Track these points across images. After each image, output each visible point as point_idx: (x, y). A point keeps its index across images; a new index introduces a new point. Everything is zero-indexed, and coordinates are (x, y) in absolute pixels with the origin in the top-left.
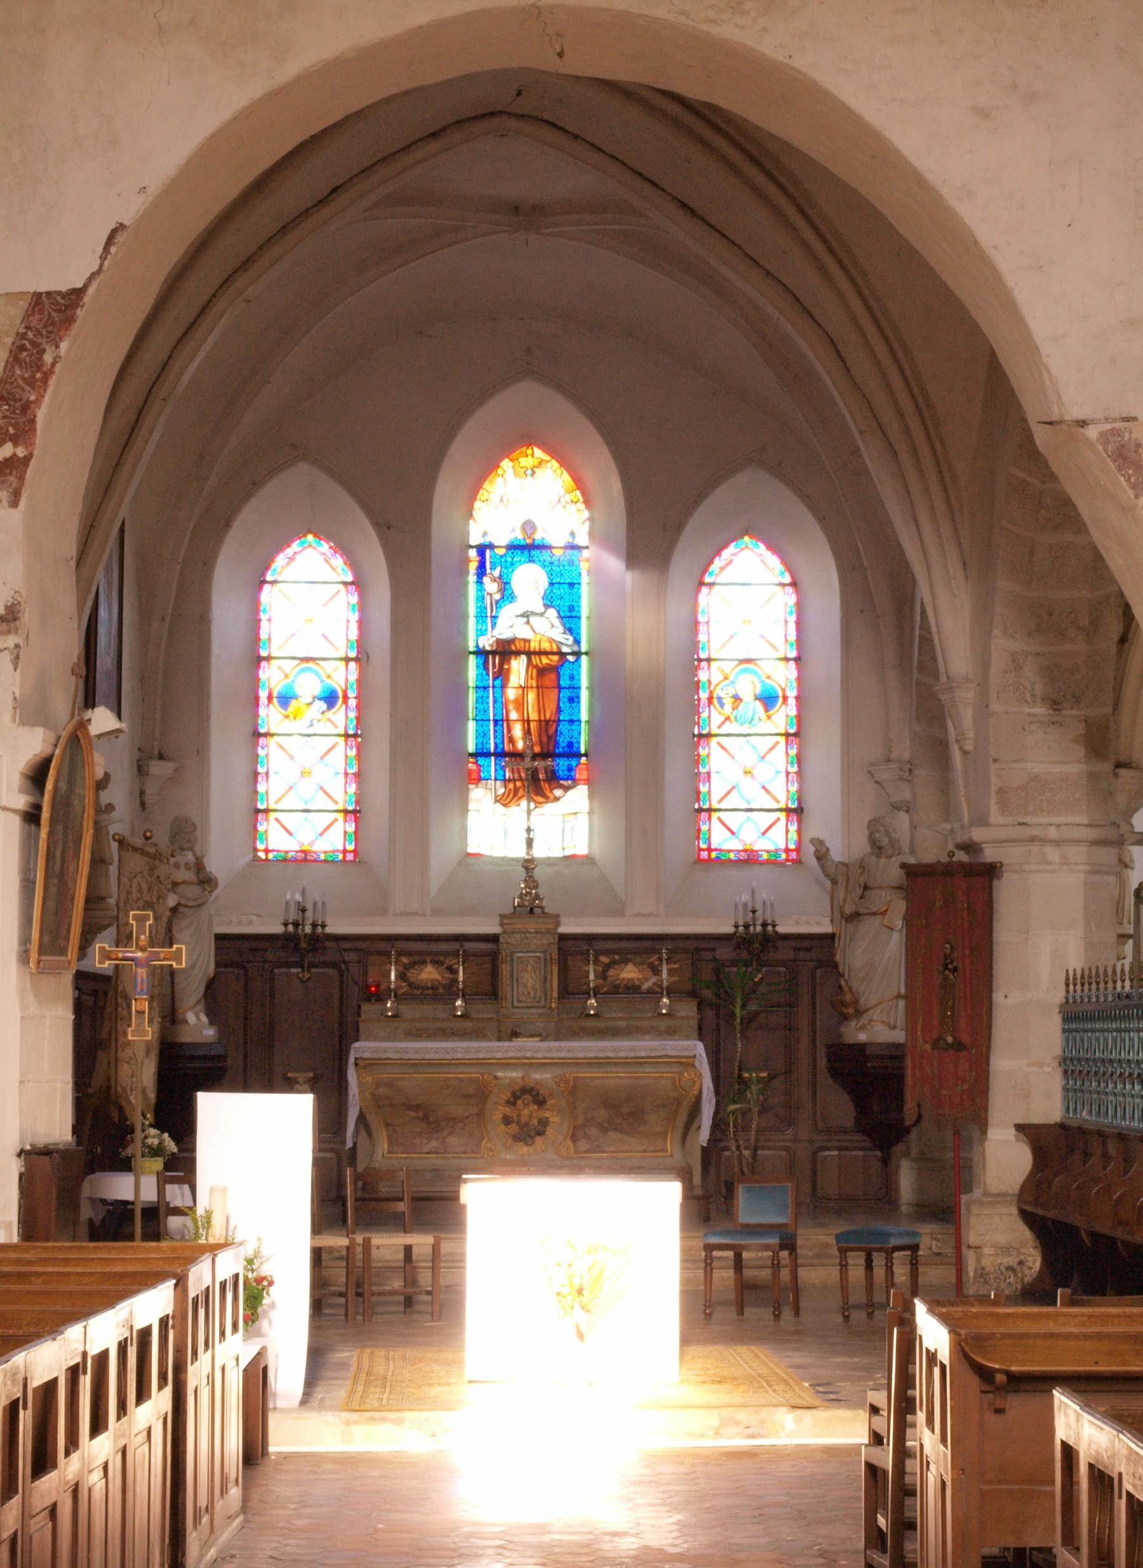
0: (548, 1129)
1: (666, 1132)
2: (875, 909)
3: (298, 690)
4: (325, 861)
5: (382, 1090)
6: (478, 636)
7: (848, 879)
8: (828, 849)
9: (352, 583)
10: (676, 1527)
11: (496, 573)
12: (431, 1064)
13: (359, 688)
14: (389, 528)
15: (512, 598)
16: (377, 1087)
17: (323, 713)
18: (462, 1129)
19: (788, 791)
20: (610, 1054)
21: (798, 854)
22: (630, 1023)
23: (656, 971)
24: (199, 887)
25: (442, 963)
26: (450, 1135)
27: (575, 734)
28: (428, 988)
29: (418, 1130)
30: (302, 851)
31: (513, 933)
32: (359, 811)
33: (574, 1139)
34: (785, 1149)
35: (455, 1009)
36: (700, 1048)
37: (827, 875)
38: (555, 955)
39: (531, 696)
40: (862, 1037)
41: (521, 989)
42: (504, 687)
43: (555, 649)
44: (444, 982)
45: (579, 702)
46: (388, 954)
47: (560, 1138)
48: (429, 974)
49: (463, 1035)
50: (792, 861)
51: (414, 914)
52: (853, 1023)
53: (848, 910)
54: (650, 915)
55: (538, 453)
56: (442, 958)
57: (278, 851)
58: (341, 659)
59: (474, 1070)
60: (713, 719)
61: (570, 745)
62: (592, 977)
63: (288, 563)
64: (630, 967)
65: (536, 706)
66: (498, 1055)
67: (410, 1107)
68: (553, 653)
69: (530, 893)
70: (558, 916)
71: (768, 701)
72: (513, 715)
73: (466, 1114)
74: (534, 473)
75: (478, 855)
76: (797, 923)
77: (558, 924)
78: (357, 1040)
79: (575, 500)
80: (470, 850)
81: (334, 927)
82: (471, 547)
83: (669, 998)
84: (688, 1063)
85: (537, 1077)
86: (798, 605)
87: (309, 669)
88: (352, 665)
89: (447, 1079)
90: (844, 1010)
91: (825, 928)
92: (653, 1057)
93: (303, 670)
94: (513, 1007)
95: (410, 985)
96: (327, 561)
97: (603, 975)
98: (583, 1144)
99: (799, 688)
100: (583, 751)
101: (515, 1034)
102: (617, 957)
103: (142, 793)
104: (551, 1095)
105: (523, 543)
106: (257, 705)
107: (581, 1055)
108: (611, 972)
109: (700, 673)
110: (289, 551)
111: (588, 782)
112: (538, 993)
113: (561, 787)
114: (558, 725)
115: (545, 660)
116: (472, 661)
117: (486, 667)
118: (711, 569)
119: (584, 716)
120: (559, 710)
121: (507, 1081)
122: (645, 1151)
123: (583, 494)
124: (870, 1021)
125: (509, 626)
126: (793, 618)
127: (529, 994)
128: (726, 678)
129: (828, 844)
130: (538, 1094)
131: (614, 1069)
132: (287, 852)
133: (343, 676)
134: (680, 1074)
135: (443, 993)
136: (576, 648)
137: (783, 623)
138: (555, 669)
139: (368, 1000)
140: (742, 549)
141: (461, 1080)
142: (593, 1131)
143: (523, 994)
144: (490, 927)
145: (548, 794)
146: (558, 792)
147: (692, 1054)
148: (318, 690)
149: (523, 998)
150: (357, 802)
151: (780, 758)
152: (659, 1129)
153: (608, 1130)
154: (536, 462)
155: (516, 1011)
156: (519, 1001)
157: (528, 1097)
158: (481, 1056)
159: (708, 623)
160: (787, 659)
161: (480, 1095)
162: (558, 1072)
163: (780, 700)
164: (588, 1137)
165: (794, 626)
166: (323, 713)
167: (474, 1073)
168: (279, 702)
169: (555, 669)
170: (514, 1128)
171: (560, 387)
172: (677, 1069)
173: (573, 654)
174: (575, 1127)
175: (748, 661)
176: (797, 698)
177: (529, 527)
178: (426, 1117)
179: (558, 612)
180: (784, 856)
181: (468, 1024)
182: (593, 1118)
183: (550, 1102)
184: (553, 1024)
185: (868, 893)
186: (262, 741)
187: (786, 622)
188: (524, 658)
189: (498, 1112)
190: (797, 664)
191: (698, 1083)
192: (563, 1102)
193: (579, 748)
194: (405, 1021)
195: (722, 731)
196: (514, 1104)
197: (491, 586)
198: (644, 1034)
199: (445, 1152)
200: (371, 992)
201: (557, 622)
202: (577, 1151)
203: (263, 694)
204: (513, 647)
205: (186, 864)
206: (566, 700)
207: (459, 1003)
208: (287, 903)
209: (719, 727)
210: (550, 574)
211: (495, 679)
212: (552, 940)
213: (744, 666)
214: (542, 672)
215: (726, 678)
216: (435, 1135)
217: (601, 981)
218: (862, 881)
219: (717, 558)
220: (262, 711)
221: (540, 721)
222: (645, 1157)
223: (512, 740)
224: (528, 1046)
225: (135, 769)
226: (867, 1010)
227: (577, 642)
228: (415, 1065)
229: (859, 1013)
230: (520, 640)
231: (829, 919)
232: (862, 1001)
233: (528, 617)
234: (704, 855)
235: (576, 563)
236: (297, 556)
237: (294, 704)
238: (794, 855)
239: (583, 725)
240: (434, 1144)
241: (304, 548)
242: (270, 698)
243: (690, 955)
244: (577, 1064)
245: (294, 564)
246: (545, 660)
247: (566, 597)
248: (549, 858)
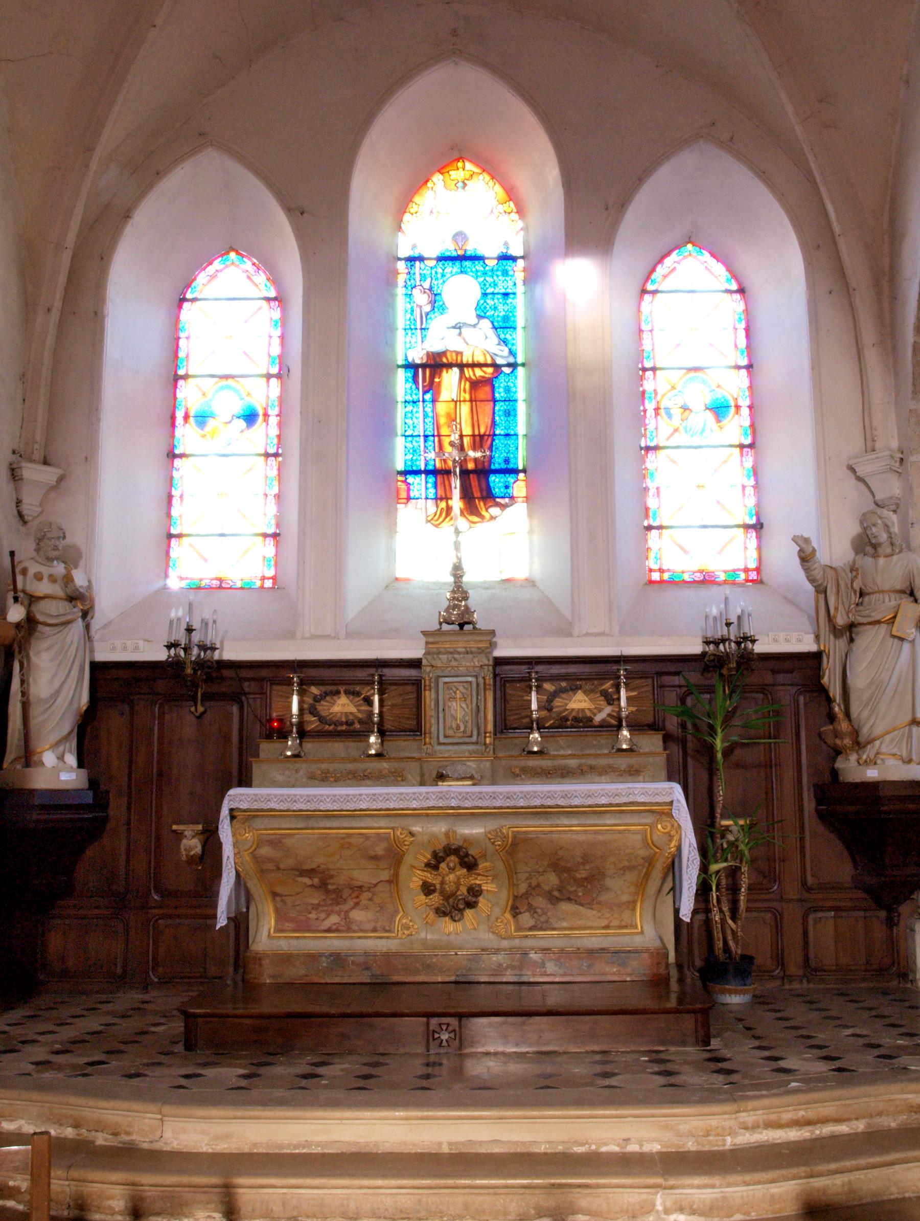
0: (481, 899)
1: (635, 902)
2: (877, 617)
3: (216, 408)
4: (242, 588)
5: (265, 851)
7: (838, 586)
8: (814, 550)
9: (275, 299)
12: (328, 815)
13: (281, 405)
14: (302, 214)
15: (443, 308)
16: (258, 846)
17: (242, 431)
18: (370, 900)
19: (683, 572)
20: (561, 802)
21: (758, 573)
22: (583, 761)
23: (612, 699)
24: (66, 603)
25: (358, 694)
26: (353, 908)
27: (512, 448)
28: (342, 724)
29: (315, 901)
30: (216, 579)
31: (439, 653)
32: (279, 535)
33: (515, 912)
34: (768, 910)
35: (369, 746)
36: (676, 792)
37: (812, 580)
38: (490, 681)
39: (465, 409)
40: (872, 774)
41: (449, 721)
42: (434, 401)
43: (489, 361)
44: (360, 715)
45: (515, 416)
46: (289, 683)
47: (497, 911)
48: (342, 706)
49: (378, 778)
50: (752, 581)
51: (328, 637)
52: (853, 757)
53: (841, 620)
54: (602, 634)
55: (469, 166)
56: (358, 688)
57: (192, 579)
58: (262, 376)
59: (383, 823)
60: (659, 430)
61: (507, 461)
62: (534, 706)
63: (209, 281)
64: (580, 695)
66: (414, 804)
67: (302, 873)
68: (486, 365)
69: (458, 607)
70: (493, 633)
71: (718, 411)
73: (375, 882)
74: (465, 185)
75: (407, 580)
76: (775, 641)
77: (493, 645)
78: (245, 781)
80: (398, 576)
81: (231, 652)
82: (400, 259)
83: (630, 731)
84: (664, 811)
85: (467, 831)
86: (746, 311)
87: (228, 387)
88: (274, 381)
89: (349, 836)
90: (838, 742)
91: (807, 645)
92: (617, 805)
93: (222, 388)
94: (439, 744)
95: (321, 719)
96: (249, 278)
97: (546, 706)
98: (526, 919)
99: (752, 396)
100: (521, 467)
101: (441, 777)
102: (564, 684)
103: (19, 502)
104: (484, 856)
105: (454, 254)
106: (173, 426)
107: (522, 803)
108: (558, 702)
109: (645, 383)
110: (211, 269)
112: (469, 725)
113: (498, 505)
114: (493, 440)
115: (479, 372)
118: (653, 277)
119: (521, 428)
120: (493, 423)
121: (426, 837)
122: (607, 927)
123: (516, 205)
124: (878, 753)
125: (440, 338)
126: (743, 325)
127: (458, 727)
128: (673, 388)
129: (815, 544)
130: (467, 855)
131: (566, 821)
132: (201, 580)
133: (263, 395)
134: (652, 826)
135: (352, 731)
136: (511, 360)
137: (732, 331)
138: (489, 382)
139: (269, 737)
140: (685, 257)
141: (367, 837)
142: (540, 902)
143: (451, 727)
144: (413, 650)
145: (484, 513)
146: (494, 511)
147: (668, 800)
148: (238, 407)
149: (450, 732)
150: (277, 526)
151: (736, 470)
152: (625, 898)
153: (558, 900)
154: (467, 175)
155: (442, 748)
156: (446, 736)
157: (453, 860)
158: (392, 805)
159: (651, 331)
160: (738, 367)
161: (394, 856)
162: (492, 825)
163: (733, 410)
164: (532, 909)
165: (743, 333)
166: (242, 431)
167: (382, 827)
168: (196, 422)
169: (489, 382)
170: (436, 899)
171: (487, 65)
172: (649, 819)
174: (516, 897)
175: (696, 369)
176: (750, 407)
178: (323, 885)
179: (492, 323)
180: (743, 576)
181: (384, 765)
182: (538, 885)
183: (482, 865)
184: (488, 764)
185: (866, 599)
186: (177, 462)
187: (736, 329)
188: (456, 370)
189: (414, 879)
190: (749, 372)
191: (676, 838)
192: (500, 865)
193: (516, 463)
194: (306, 761)
195: (671, 443)
196: (436, 867)
197: (421, 299)
198: (600, 774)
199: (349, 930)
200: (272, 728)
201: (491, 333)
202: (519, 928)
203: (180, 415)
204: (445, 360)
205: (51, 576)
206: (501, 413)
207: (372, 739)
208: (171, 622)
209: (668, 439)
210: (483, 285)
211: (425, 392)
212: (485, 661)
213: (692, 374)
214: (475, 385)
215: (673, 388)
216: (337, 908)
217: (544, 713)
218: (857, 585)
219: (659, 266)
220: (178, 432)
221: (473, 436)
222: (608, 935)
224: (454, 791)
225: (9, 473)
226: (870, 742)
228: (307, 816)
229: (859, 745)
230: (451, 352)
231: (812, 636)
232: (865, 731)
233: (460, 328)
234: (656, 576)
235: (511, 273)
236: (219, 274)
237: (211, 423)
238: (753, 575)
239: (520, 438)
240: (334, 919)
241: (227, 267)
242: (186, 417)
243: (650, 681)
244: (516, 813)
245: (215, 281)
246: (479, 372)
247: (500, 307)
248: (485, 582)
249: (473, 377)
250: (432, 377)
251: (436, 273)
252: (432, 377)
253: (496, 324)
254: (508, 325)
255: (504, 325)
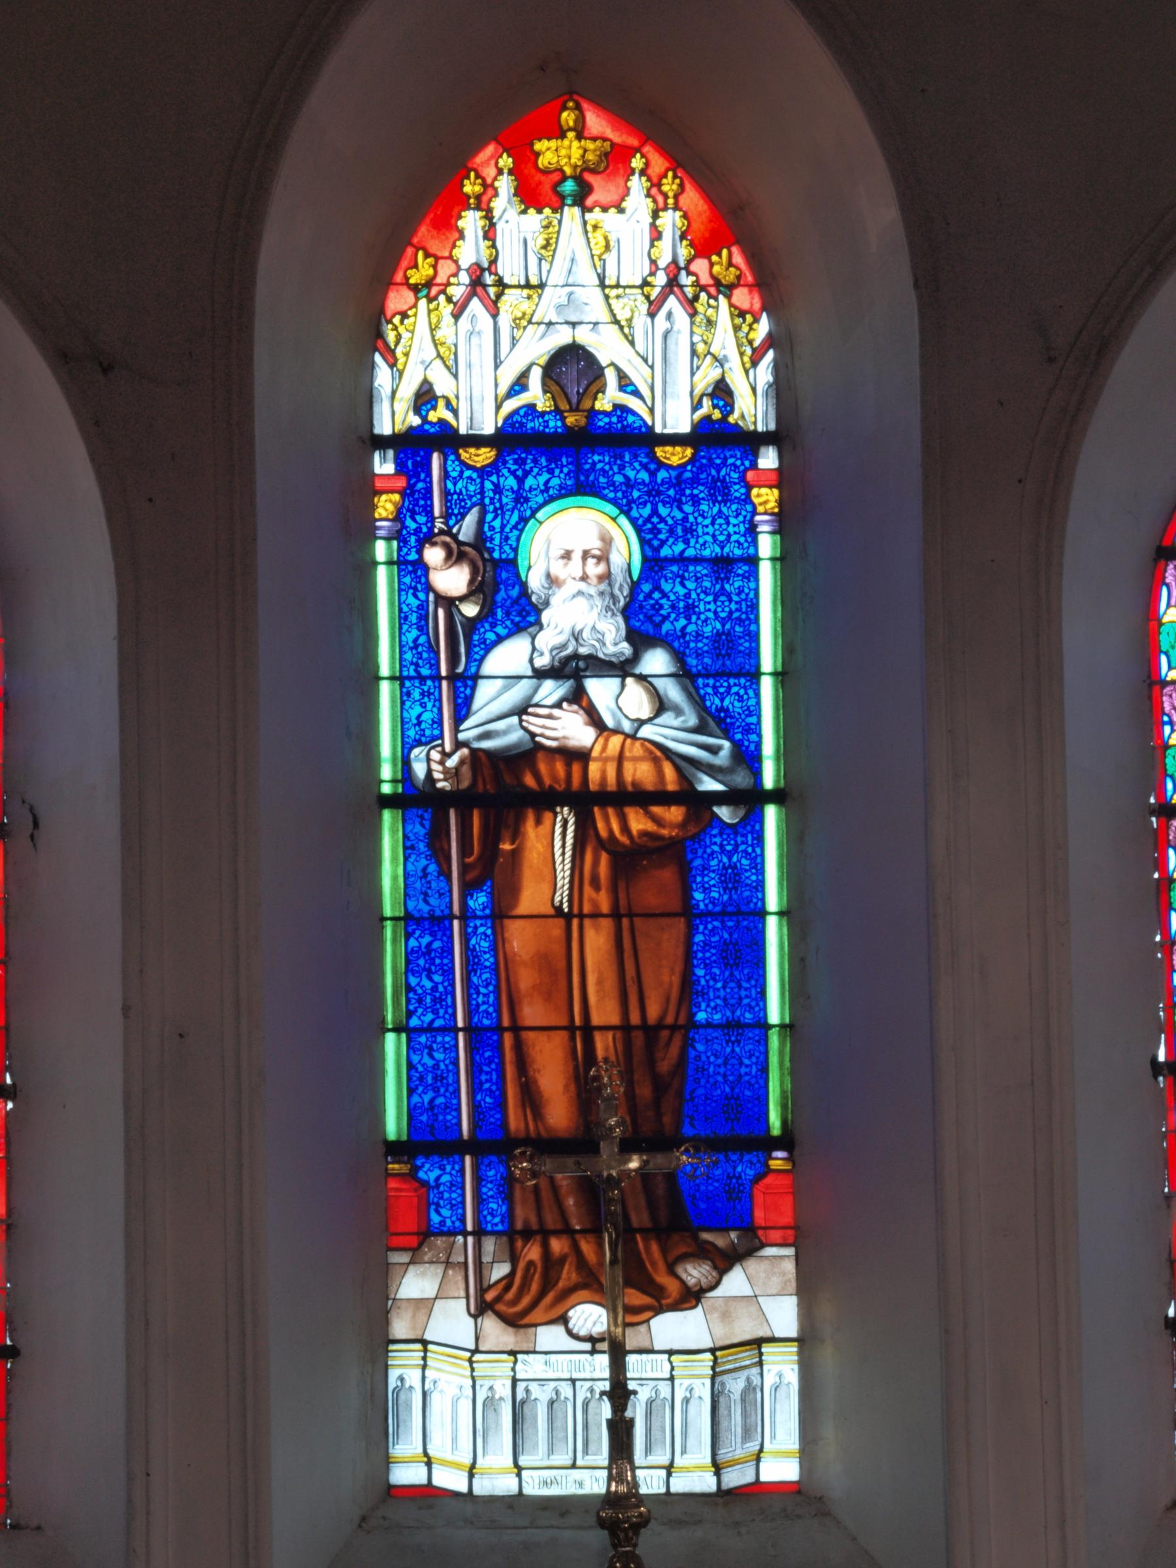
6: (407, 747)
11: (467, 528)
14: (106, 370)
39: (597, 942)
42: (499, 914)
65: (611, 982)
68: (663, 797)
72: (532, 1013)
79: (730, 276)
111: (796, 1236)
113: (703, 1252)
114: (687, 1044)
115: (638, 822)
116: (390, 831)
117: (439, 854)
119: (775, 1012)
123: (752, 258)
136: (742, 779)
169: (673, 852)
173: (728, 798)
177: (572, 367)
201: (672, 691)
204: (529, 781)
211: (468, 889)
214: (629, 860)
221: (625, 1028)
223: (531, 1097)
227: (748, 757)
233: (578, 677)
246: (638, 822)
247: (706, 606)
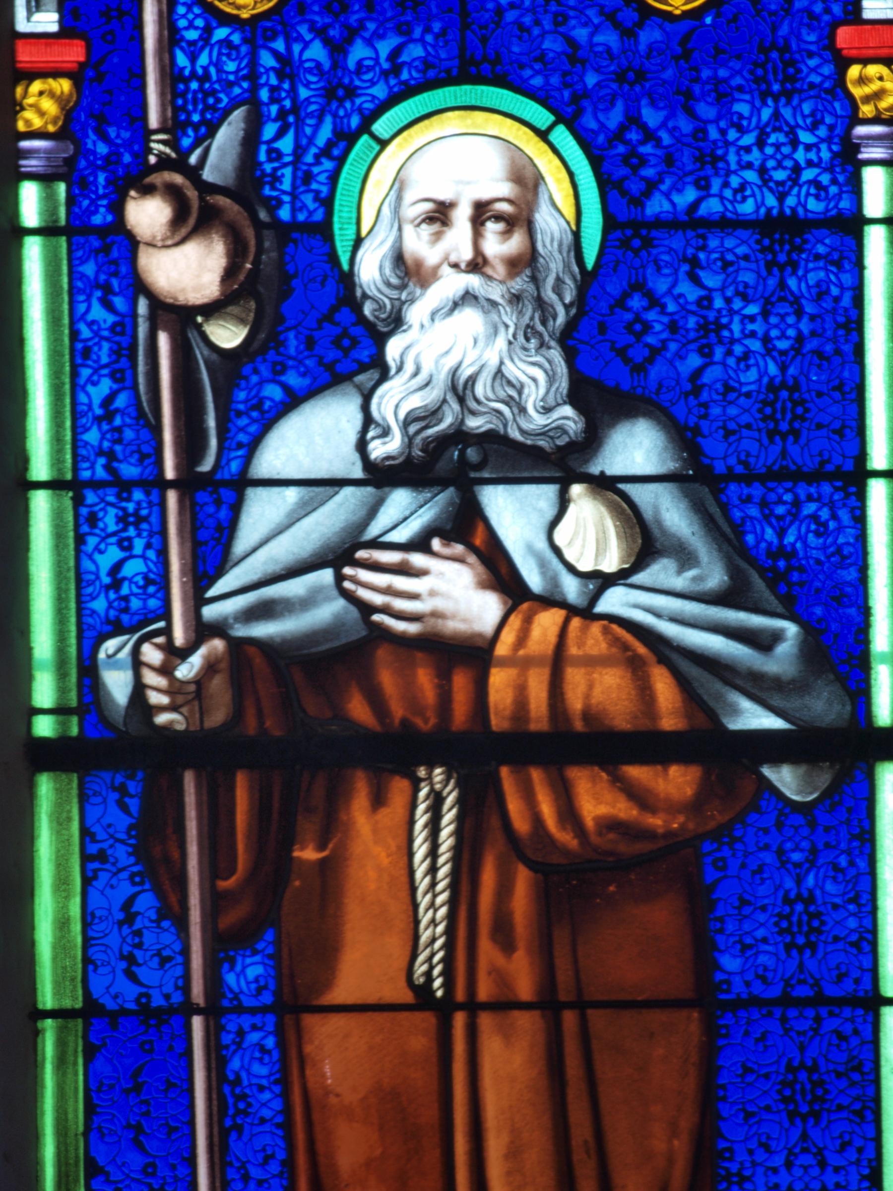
10: (656, 242)
39: (506, 1064)
42: (294, 1001)
68: (652, 746)
136: (824, 706)
204: (358, 709)
211: (223, 947)
246: (597, 800)
249: (565, 838)
250: (276, 834)
251: (288, 67)
252: (276, 834)
253: (713, 446)
254: (800, 455)
255: (767, 456)
